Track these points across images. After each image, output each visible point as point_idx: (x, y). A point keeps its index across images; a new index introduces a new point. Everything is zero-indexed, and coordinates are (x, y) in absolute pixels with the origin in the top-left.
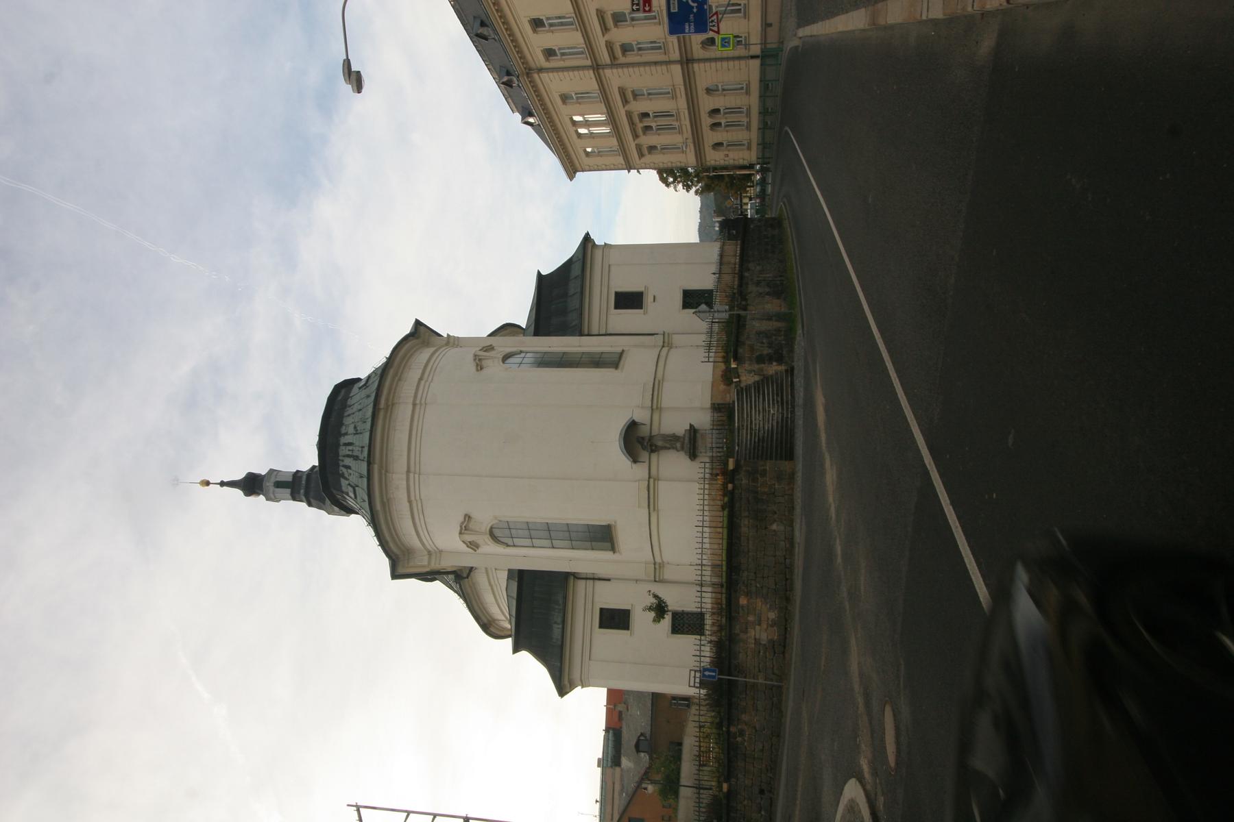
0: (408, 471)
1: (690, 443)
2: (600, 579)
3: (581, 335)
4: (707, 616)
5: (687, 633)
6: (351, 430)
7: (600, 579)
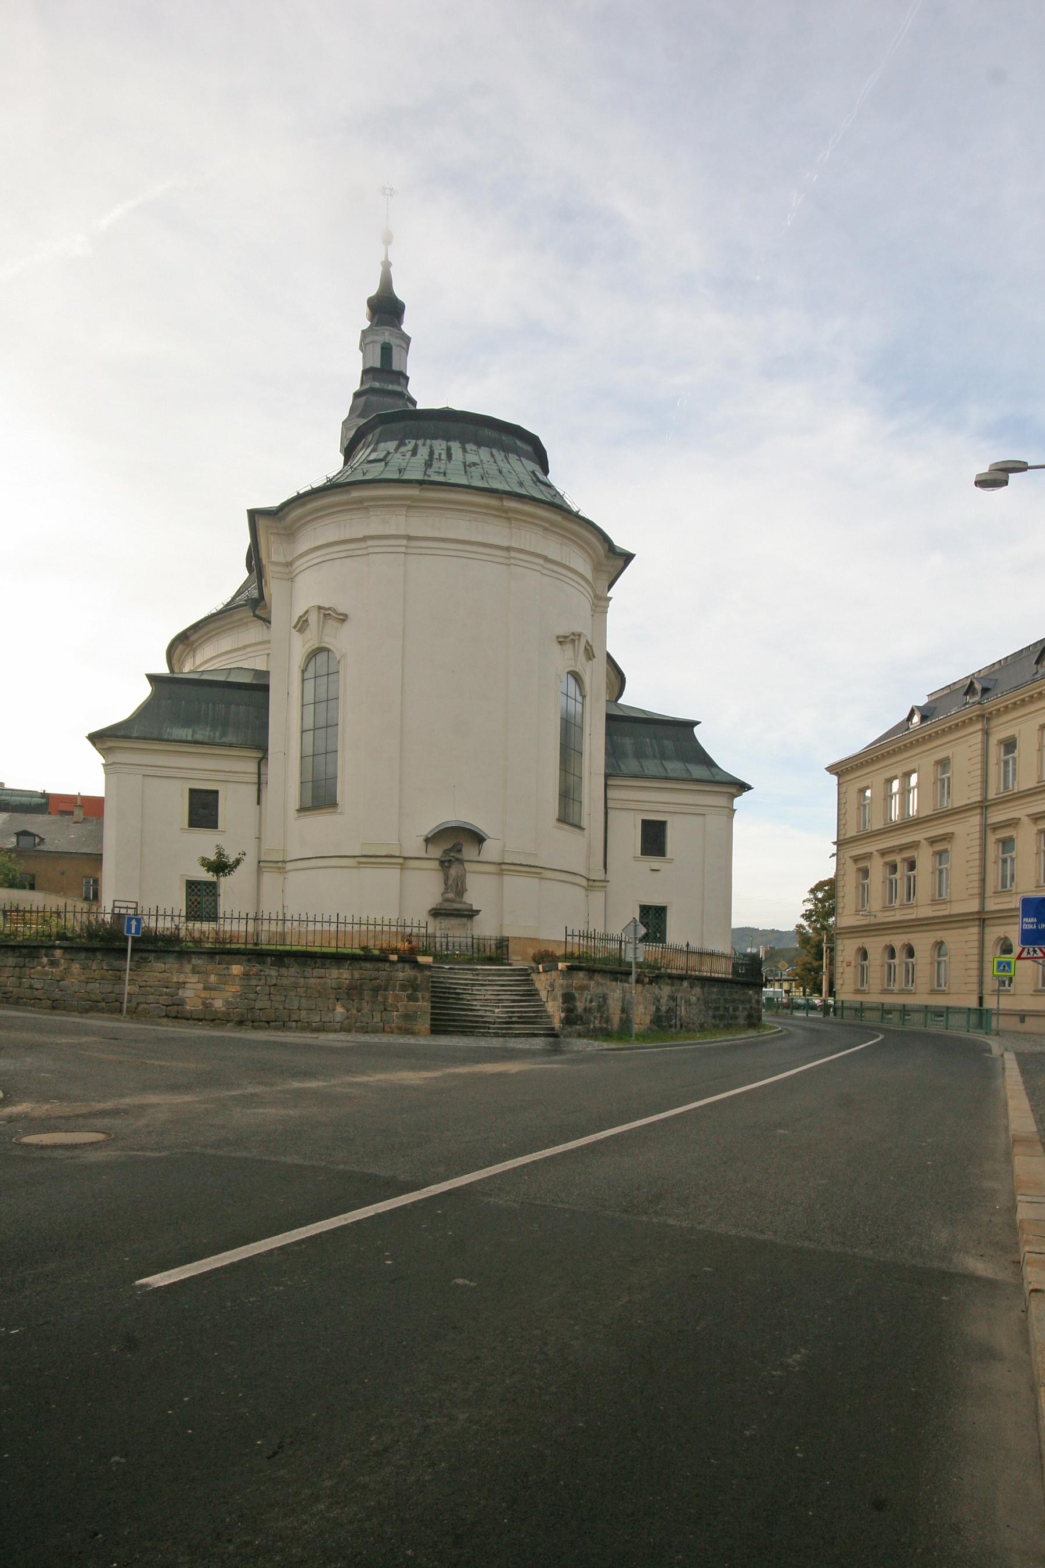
0: (409, 538)
1: (453, 910)
2: (259, 791)
5: (188, 900)
6: (471, 458)
7: (259, 791)
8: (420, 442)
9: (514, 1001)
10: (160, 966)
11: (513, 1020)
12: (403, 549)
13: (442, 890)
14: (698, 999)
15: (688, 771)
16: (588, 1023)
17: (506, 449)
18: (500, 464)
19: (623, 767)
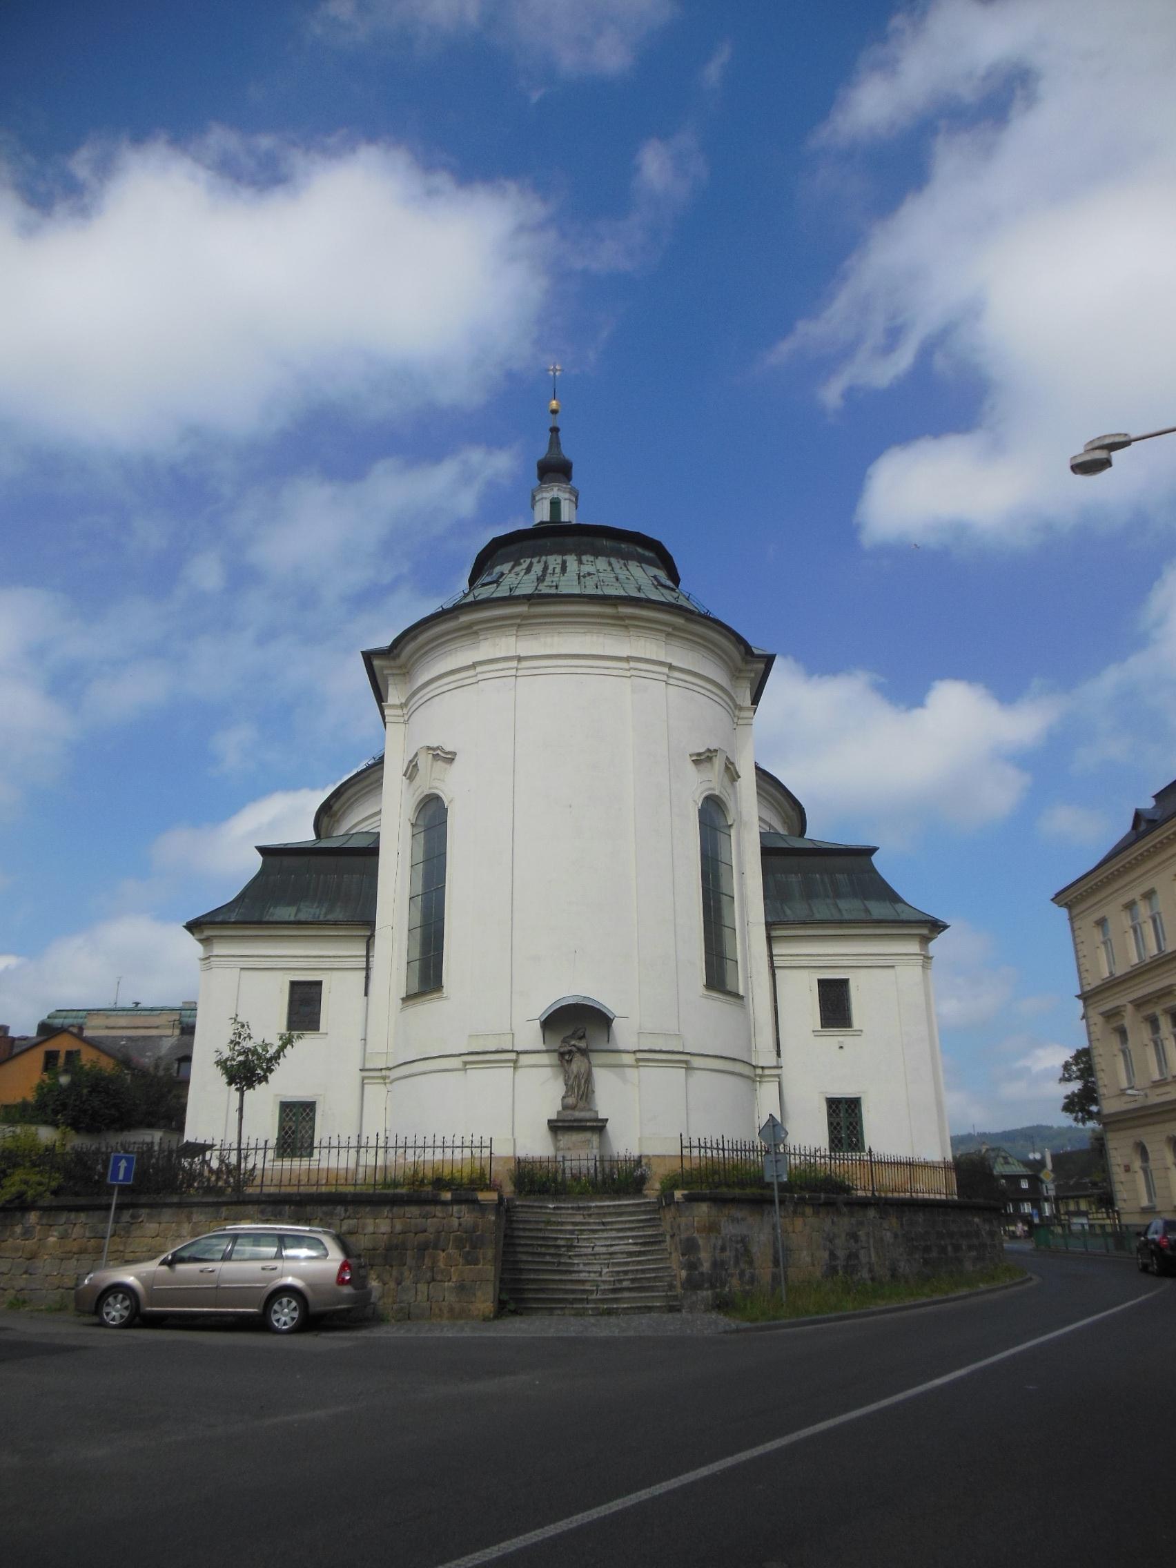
0: (519, 659)
1: (577, 1121)
2: (367, 978)
3: (769, 926)
4: (305, 1163)
5: (282, 1128)
6: (586, 569)
7: (367, 978)
8: (535, 560)
9: (630, 1254)
10: (152, 1227)
11: (625, 1284)
12: (513, 672)
13: (563, 1093)
14: (896, 1236)
15: (867, 911)
16: (723, 1285)
17: (626, 557)
18: (618, 571)
19: (788, 912)
